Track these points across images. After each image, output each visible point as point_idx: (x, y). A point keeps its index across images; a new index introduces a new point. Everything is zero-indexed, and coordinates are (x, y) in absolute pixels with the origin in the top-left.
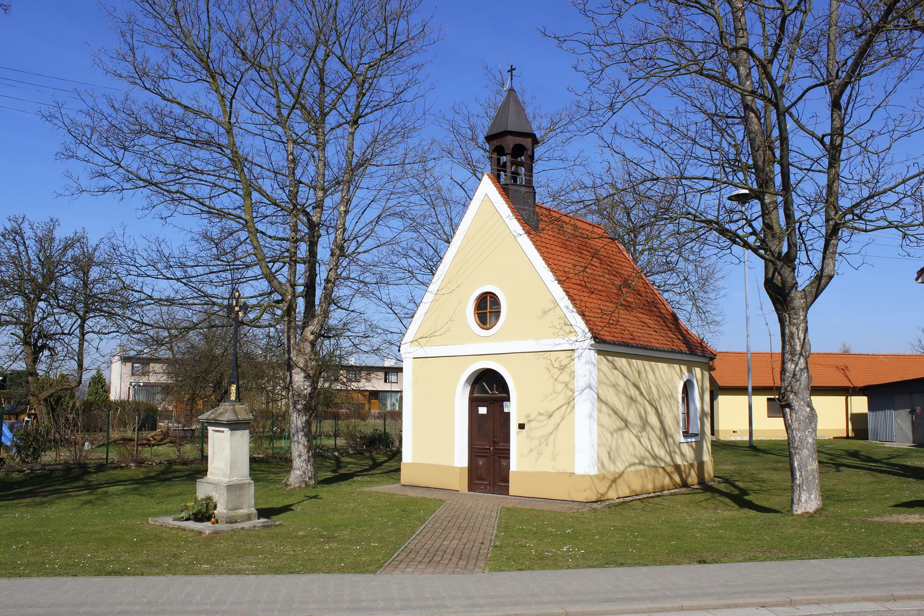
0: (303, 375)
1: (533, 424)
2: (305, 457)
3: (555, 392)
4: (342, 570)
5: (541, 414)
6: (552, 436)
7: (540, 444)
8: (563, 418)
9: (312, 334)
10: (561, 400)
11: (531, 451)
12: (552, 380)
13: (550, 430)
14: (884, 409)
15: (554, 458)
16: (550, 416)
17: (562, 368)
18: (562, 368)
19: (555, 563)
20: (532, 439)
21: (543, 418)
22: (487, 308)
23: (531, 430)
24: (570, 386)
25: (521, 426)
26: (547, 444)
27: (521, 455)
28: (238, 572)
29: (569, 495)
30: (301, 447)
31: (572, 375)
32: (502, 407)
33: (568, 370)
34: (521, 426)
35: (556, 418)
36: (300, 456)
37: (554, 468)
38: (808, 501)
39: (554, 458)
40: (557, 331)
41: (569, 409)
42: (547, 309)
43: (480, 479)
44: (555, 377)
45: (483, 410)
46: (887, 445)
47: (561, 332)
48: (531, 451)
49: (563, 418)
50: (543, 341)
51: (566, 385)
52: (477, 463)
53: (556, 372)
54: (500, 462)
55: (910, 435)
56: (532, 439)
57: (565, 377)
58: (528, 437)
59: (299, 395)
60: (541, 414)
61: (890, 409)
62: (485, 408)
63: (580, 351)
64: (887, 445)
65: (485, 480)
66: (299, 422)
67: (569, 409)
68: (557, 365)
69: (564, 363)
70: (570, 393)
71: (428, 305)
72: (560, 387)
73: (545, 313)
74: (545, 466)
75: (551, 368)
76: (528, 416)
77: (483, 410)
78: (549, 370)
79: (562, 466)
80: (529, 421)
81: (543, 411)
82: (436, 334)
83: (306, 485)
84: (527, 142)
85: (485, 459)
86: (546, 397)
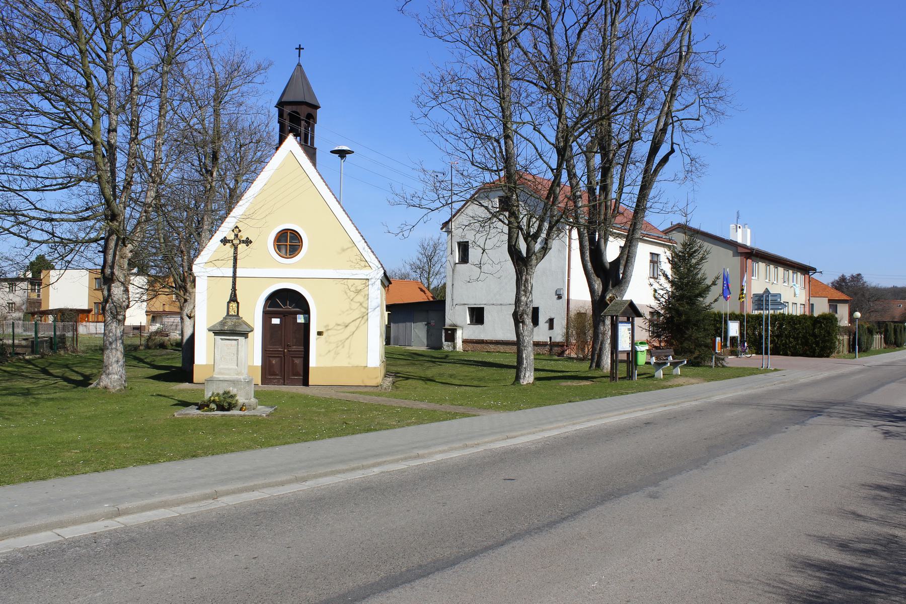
0: (122, 288)
1: (330, 332)
2: (121, 363)
4: (360, 432)
6: (348, 341)
9: (131, 251)
10: (356, 314)
14: (404, 321)
17: (358, 292)
18: (358, 292)
19: (225, 449)
21: (339, 327)
22: (288, 242)
23: (329, 336)
24: (364, 305)
25: (320, 333)
28: (622, 394)
30: (119, 353)
31: (367, 297)
33: (363, 293)
34: (320, 333)
35: (352, 327)
36: (117, 362)
38: (528, 377)
41: (363, 322)
45: (276, 321)
46: (408, 348)
47: (357, 266)
53: (352, 295)
55: (425, 341)
57: (360, 298)
61: (410, 321)
63: (373, 280)
64: (408, 348)
65: (276, 375)
66: (118, 331)
67: (363, 322)
68: (353, 289)
69: (359, 288)
70: (364, 310)
73: (344, 250)
74: (342, 361)
76: (327, 326)
77: (276, 321)
79: (357, 361)
84: (303, 111)
85: (278, 359)
86: (343, 312)
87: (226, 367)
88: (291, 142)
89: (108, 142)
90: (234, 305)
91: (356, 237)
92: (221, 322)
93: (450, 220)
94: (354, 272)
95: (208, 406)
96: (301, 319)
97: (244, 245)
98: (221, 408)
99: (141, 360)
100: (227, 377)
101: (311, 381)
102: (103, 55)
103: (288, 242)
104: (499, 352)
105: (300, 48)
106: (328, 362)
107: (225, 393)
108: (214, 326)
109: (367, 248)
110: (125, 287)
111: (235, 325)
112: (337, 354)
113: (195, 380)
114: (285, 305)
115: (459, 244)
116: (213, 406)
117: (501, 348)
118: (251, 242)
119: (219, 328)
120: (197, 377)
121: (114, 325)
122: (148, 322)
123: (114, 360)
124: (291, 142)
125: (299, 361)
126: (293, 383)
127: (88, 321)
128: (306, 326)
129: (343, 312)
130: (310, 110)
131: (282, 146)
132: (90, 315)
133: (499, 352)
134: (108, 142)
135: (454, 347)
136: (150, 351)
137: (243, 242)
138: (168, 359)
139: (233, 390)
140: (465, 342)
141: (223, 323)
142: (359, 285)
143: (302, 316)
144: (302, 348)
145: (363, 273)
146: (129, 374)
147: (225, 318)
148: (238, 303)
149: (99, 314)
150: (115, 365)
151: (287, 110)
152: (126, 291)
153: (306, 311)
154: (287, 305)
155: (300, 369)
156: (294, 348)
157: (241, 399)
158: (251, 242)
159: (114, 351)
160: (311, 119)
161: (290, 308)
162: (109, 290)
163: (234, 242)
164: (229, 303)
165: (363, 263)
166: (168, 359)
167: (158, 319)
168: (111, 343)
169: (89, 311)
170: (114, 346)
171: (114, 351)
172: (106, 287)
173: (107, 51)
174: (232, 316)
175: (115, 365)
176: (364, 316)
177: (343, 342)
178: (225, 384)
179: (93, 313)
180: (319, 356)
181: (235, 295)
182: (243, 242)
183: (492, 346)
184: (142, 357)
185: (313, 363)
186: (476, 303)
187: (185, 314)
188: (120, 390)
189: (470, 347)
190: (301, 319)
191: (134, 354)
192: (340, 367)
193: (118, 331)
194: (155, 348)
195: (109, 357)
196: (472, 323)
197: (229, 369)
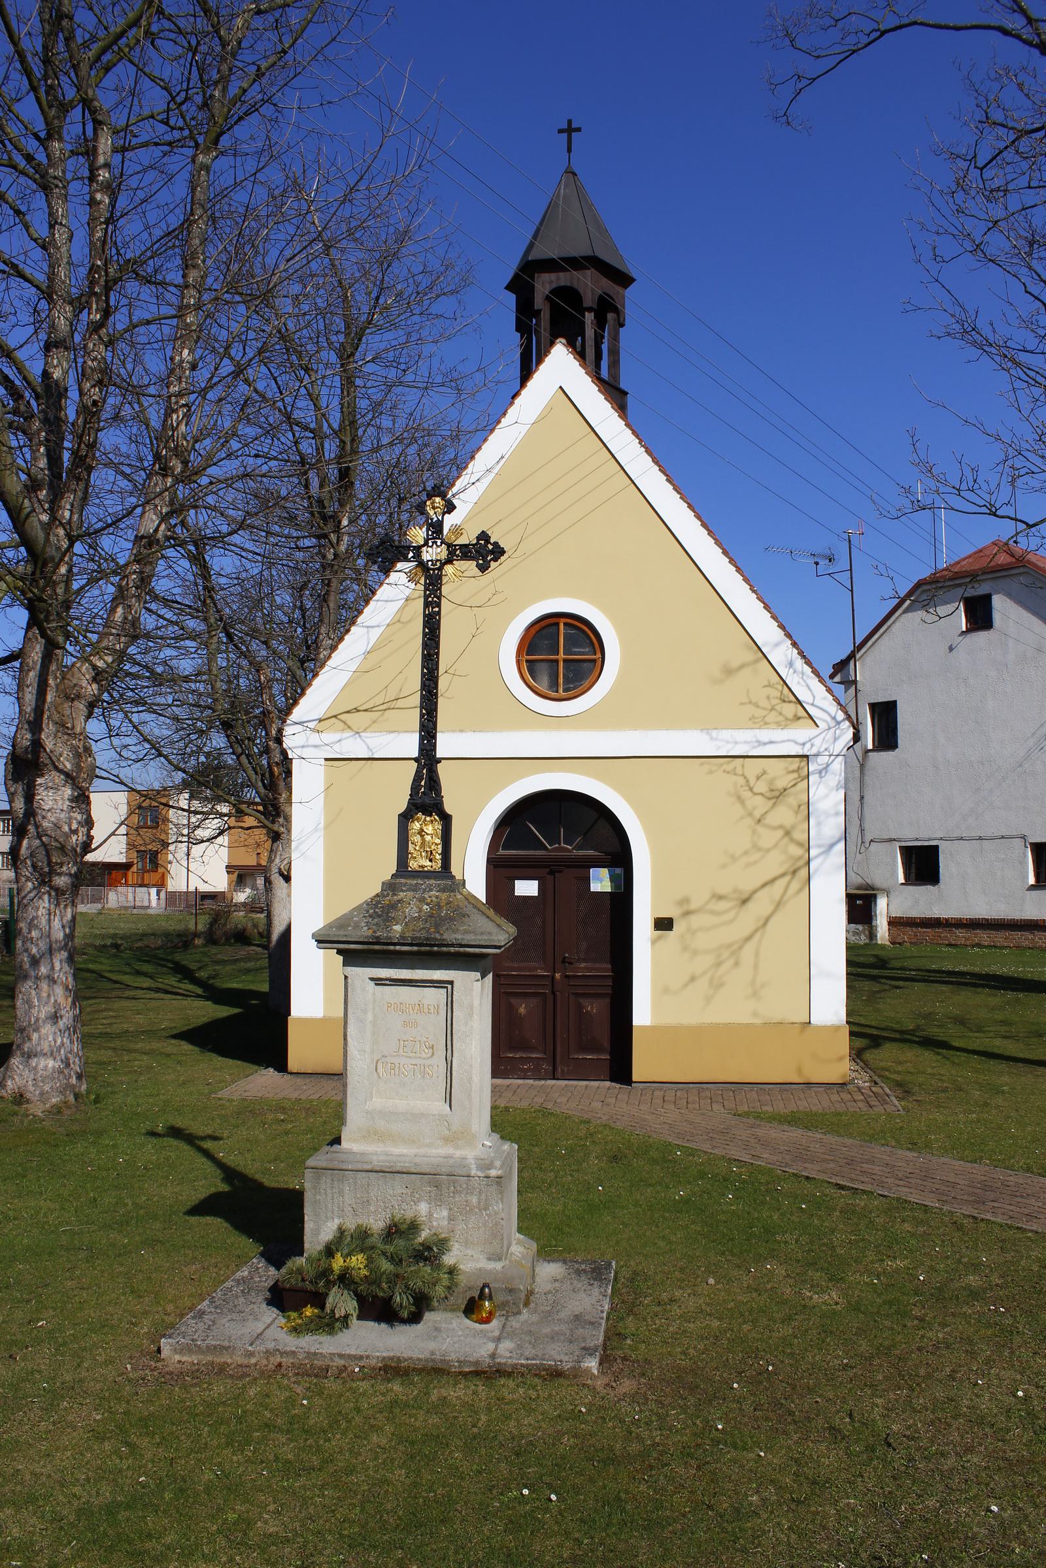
1: (695, 921)
3: (756, 847)
5: (720, 898)
6: (750, 948)
7: (719, 964)
8: (779, 905)
10: (774, 864)
11: (693, 979)
12: (749, 821)
13: (746, 933)
15: (755, 994)
16: (745, 901)
17: (777, 796)
18: (777, 796)
20: (695, 953)
21: (723, 905)
23: (692, 932)
24: (800, 836)
26: (737, 964)
27: (661, 991)
29: (799, 1071)
30: (59, 991)
31: (806, 810)
32: (587, 880)
33: (792, 800)
34: (663, 924)
35: (761, 905)
36: (55, 1017)
37: (755, 1014)
39: (755, 994)
40: (759, 713)
42: (735, 664)
43: (524, 1046)
44: (757, 814)
45: (527, 888)
47: (773, 717)
48: (693, 979)
49: (779, 905)
50: (726, 734)
51: (787, 833)
52: (511, 1009)
53: (759, 805)
54: (580, 1007)
56: (695, 953)
57: (783, 815)
58: (685, 948)
59: (62, 849)
60: (720, 898)
62: (535, 883)
63: (823, 760)
65: (532, 1049)
66: (56, 924)
67: (795, 885)
68: (761, 787)
69: (781, 784)
70: (796, 851)
71: (375, 634)
72: (769, 838)
74: (732, 1008)
75: (747, 794)
76: (685, 901)
77: (527, 888)
78: (740, 800)
80: (687, 914)
81: (721, 891)
82: (400, 704)
83: (77, 1096)
84: (589, 284)
85: (534, 1002)
86: (734, 858)
87: (401, 1104)
88: (561, 367)
89: (46, 374)
90: (427, 828)
91: (765, 629)
92: (375, 902)
93: (852, 656)
94: (764, 735)
95: (318, 1300)
96: (601, 882)
97: (470, 566)
98: (380, 1310)
99: (185, 973)
100: (401, 1152)
101: (639, 1072)
102: (32, 145)
103: (562, 654)
104: (979, 945)
105: (570, 130)
106: (691, 1012)
107: (394, 1231)
108: (341, 923)
109: (799, 663)
110: (75, 785)
111: (436, 919)
112: (717, 985)
113: (293, 1063)
114: (553, 839)
115: (873, 706)
116: (342, 1302)
117: (984, 936)
118: (498, 552)
119: (365, 932)
120: (299, 1053)
121: (44, 903)
122: (229, 884)
123: (45, 1011)
124: (561, 367)
125: (595, 1008)
126: (581, 1072)
127: (127, 885)
128: (622, 899)
129: (734, 858)
130: (606, 285)
131: (530, 384)
132: (130, 874)
133: (979, 945)
134: (46, 374)
135: (872, 935)
136: (214, 950)
137: (466, 552)
138: (248, 971)
139: (433, 1217)
140: (893, 922)
141: (381, 908)
142: (780, 773)
143: (604, 872)
144: (604, 969)
145: (789, 739)
146: (93, 1056)
147: (390, 887)
148: (446, 819)
149: (144, 871)
150: (47, 1029)
151: (544, 284)
152: (82, 800)
153: (619, 856)
154: (562, 835)
155: (603, 1033)
156: (583, 968)
157: (468, 1258)
158: (498, 552)
159: (44, 986)
160: (607, 309)
161: (570, 850)
162: (30, 797)
163: (428, 554)
164: (405, 818)
165: (790, 709)
166: (248, 971)
167: (249, 881)
168: (35, 962)
169: (126, 867)
170: (44, 970)
171: (44, 986)
172: (19, 788)
173: (50, 136)
174: (422, 874)
175: (47, 1029)
176: (801, 871)
177: (736, 949)
178: (397, 1187)
179: (134, 869)
180: (656, 991)
181: (434, 783)
182: (466, 552)
183: (961, 933)
184: (193, 966)
185: (642, 1015)
186: (920, 834)
187: (275, 870)
188: (57, 1110)
189: (907, 935)
190: (601, 882)
191: (178, 957)
192: (728, 1026)
193: (56, 924)
194: (227, 942)
195: (29, 1002)
196: (910, 880)
197: (415, 1117)
